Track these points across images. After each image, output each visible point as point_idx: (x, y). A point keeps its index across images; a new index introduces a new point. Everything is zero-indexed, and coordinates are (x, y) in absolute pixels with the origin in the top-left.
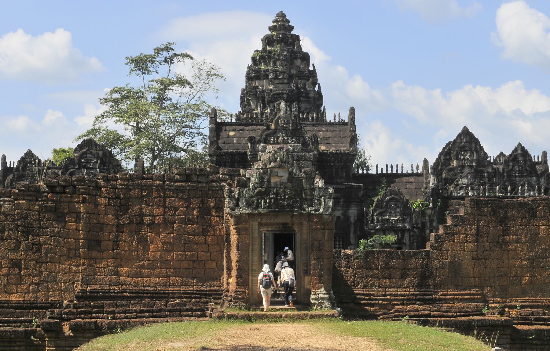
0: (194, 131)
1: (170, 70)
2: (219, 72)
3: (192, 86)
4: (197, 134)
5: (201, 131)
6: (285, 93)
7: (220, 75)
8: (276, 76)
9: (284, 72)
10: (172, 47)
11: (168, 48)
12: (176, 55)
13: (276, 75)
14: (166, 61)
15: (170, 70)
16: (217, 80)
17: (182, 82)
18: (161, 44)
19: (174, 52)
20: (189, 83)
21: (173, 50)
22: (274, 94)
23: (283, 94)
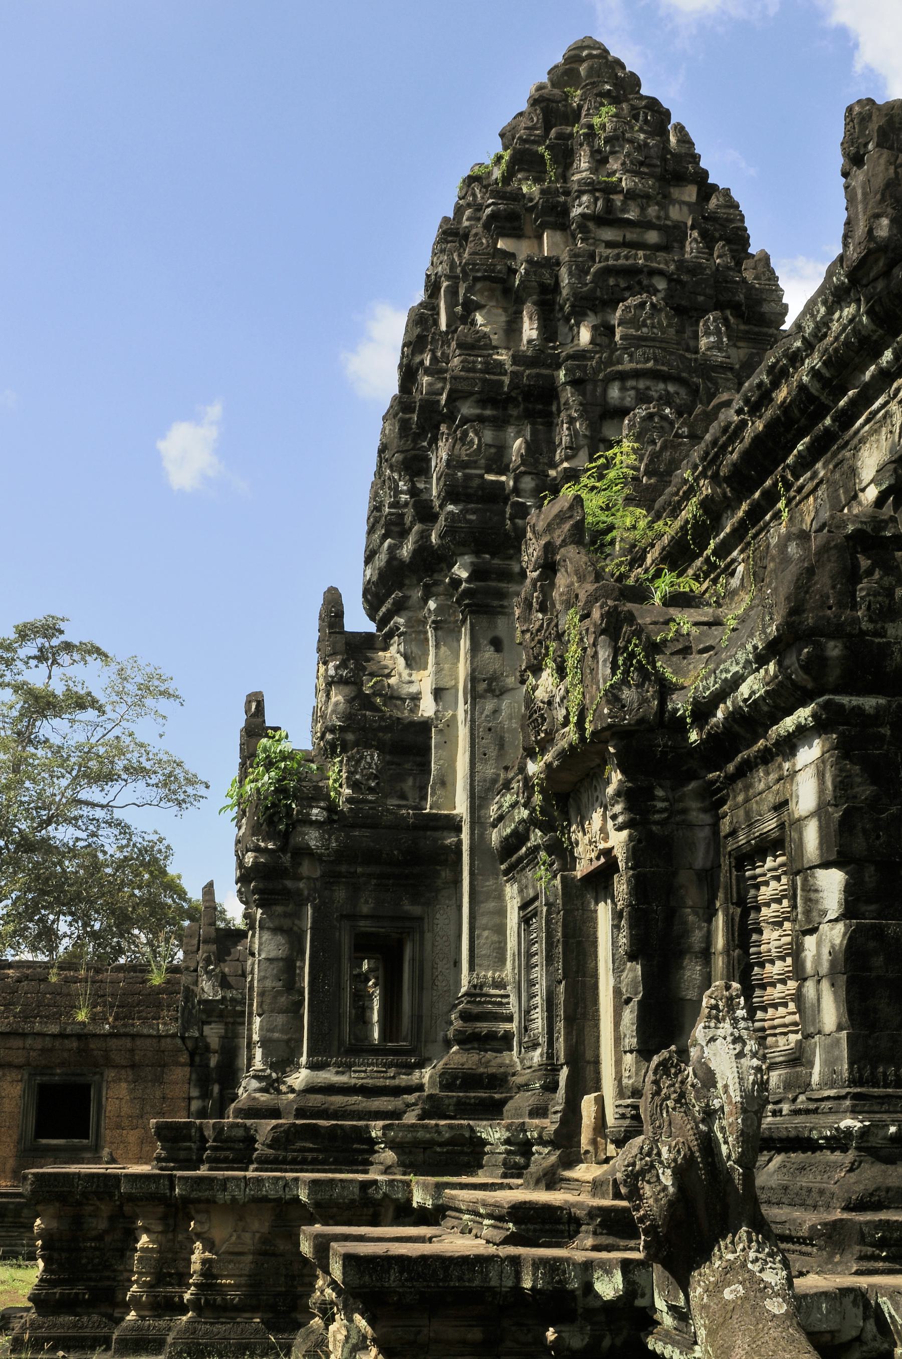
0: (99, 813)
1: (50, 677)
2: (171, 686)
3: (101, 710)
4: (106, 822)
5: (118, 814)
6: (661, 273)
7: (171, 692)
8: (609, 205)
9: (647, 197)
10: (62, 625)
11: (49, 629)
12: (68, 647)
13: (609, 203)
14: (41, 657)
15: (50, 677)
16: (163, 705)
17: (82, 702)
18: (35, 615)
19: (62, 638)
20: (94, 704)
21: (61, 632)
22: (607, 271)
23: (653, 273)
